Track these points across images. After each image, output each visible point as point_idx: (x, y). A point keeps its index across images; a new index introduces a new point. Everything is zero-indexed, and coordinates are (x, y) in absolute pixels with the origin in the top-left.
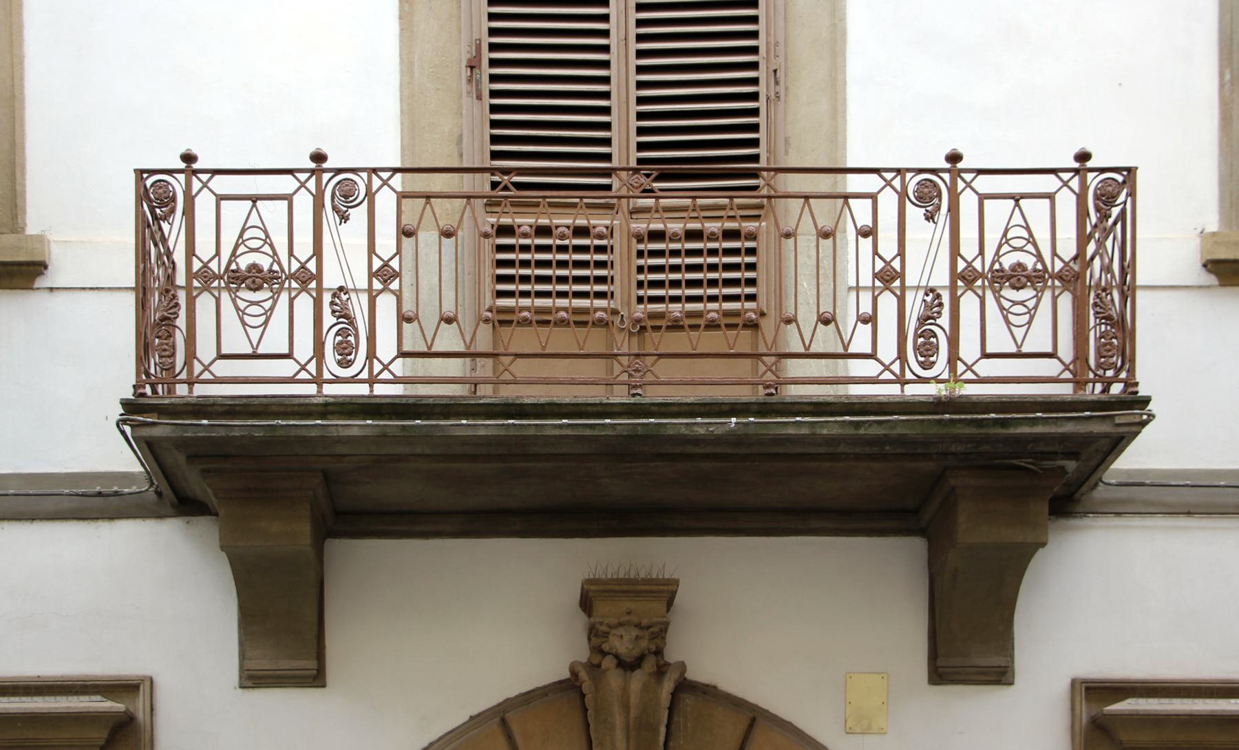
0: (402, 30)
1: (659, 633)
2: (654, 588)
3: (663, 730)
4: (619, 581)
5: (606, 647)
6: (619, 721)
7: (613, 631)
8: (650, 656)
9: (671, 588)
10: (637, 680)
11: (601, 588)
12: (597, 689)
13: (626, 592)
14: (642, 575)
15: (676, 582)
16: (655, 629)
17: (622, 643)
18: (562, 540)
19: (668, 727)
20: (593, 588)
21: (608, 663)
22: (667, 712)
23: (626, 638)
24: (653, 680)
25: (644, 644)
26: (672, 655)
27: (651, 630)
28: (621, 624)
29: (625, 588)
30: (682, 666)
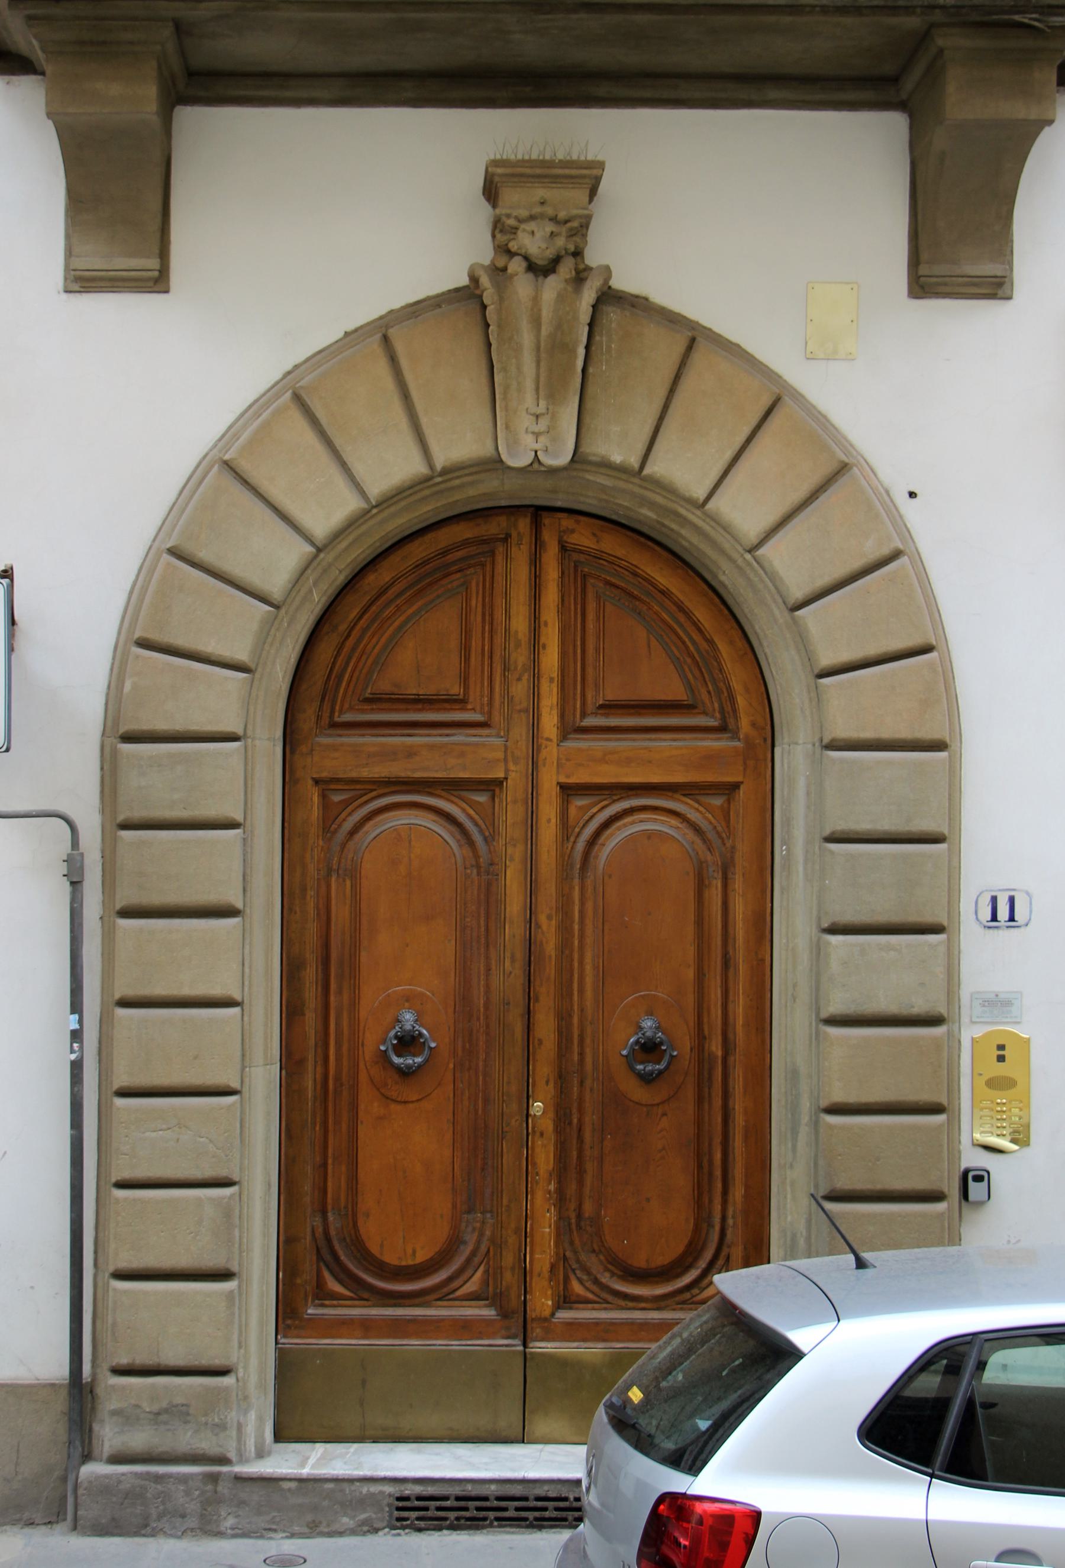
2: (574, 172)
3: (581, 351)
5: (513, 246)
6: (527, 339)
7: (523, 226)
8: (566, 259)
9: (595, 172)
10: (552, 287)
11: (509, 171)
12: (501, 299)
13: (539, 176)
15: (601, 165)
16: (575, 224)
17: (534, 242)
19: (587, 348)
20: (499, 171)
21: (516, 266)
22: (586, 329)
23: (538, 235)
24: (570, 289)
25: (561, 242)
26: (593, 257)
27: (569, 225)
28: (532, 218)
29: (538, 171)
30: (607, 271)
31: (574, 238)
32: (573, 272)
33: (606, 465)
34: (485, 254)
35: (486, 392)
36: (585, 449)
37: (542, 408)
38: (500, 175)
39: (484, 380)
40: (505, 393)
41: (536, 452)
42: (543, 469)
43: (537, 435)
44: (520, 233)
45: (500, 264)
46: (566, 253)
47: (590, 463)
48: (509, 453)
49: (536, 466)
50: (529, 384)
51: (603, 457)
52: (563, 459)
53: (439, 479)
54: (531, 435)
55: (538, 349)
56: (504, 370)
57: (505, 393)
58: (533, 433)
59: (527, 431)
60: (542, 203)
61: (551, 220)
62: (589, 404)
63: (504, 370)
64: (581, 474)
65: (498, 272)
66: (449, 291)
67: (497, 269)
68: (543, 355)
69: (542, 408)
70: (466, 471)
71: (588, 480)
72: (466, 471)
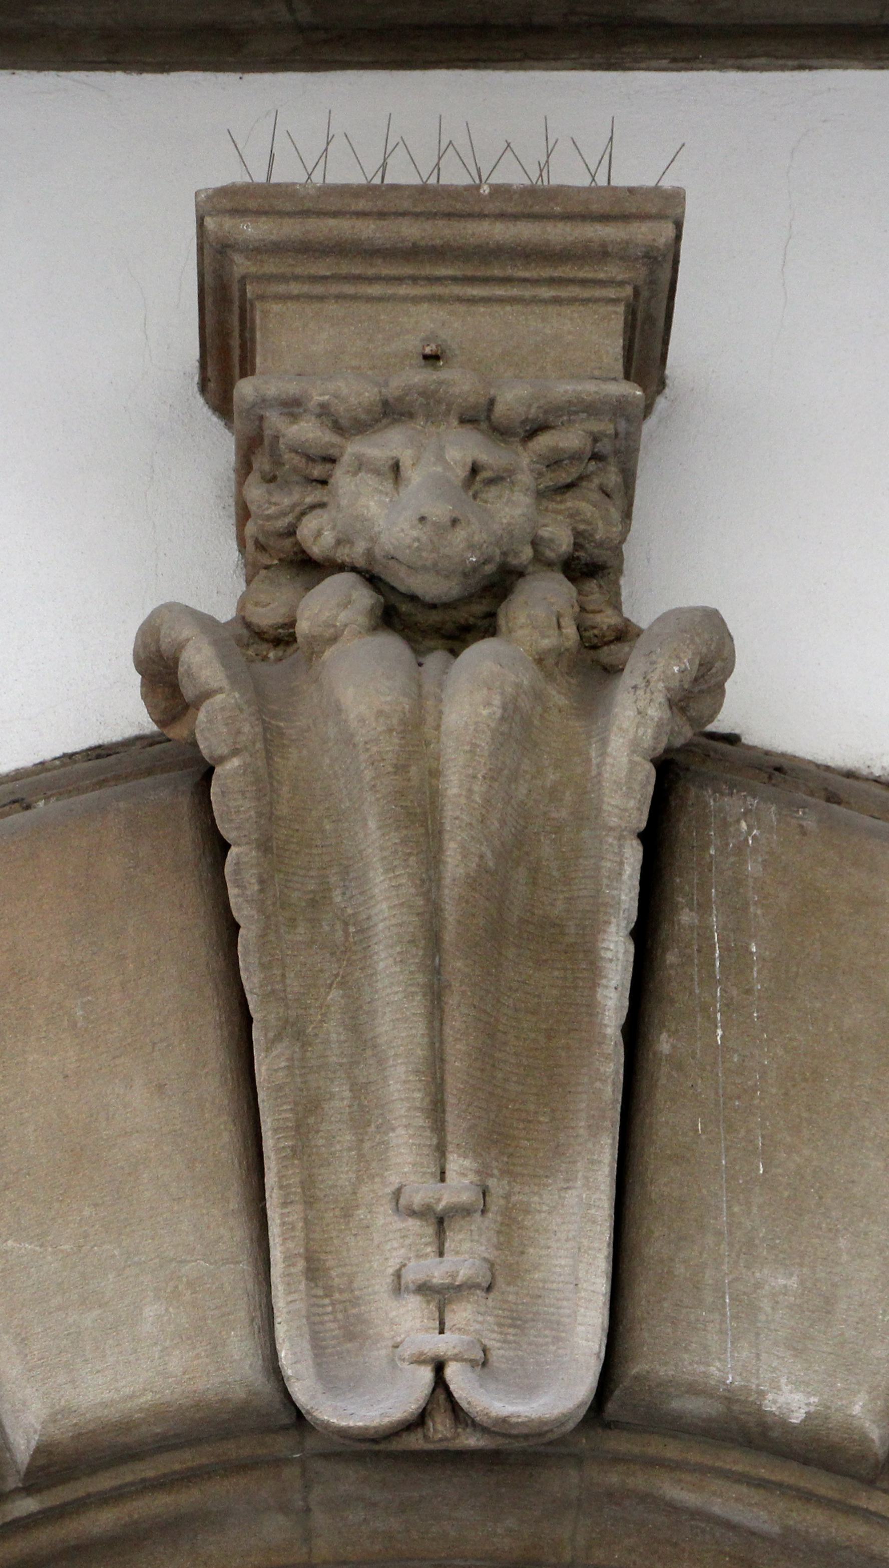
0: (538, 59)
1: (594, 463)
2: (558, 233)
3: (616, 950)
4: (378, 200)
5: (318, 535)
6: (384, 899)
7: (354, 448)
8: (546, 565)
9: (643, 233)
10: (476, 688)
11: (290, 229)
12: (272, 741)
13: (413, 253)
14: (511, 176)
15: (667, 207)
16: (569, 439)
17: (401, 505)
18: (198, 76)
19: (646, 935)
20: (250, 230)
21: (333, 605)
22: (632, 856)
23: (415, 477)
24: (557, 697)
25: (511, 509)
26: (657, 585)
27: (544, 441)
28: (392, 411)
29: (411, 231)
30: (711, 658)
31: (571, 502)
32: (570, 631)
33: (747, 1434)
34: (212, 581)
35: (222, 1138)
36: (646, 1364)
37: (460, 1181)
38: (259, 250)
39: (214, 1086)
40: (302, 1130)
41: (439, 1367)
42: (471, 1441)
43: (440, 1297)
44: (344, 481)
45: (267, 616)
46: (538, 558)
47: (678, 1428)
48: (329, 1380)
49: (441, 1427)
50: (400, 1088)
51: (730, 1398)
52: (559, 1392)
53: (28, 1505)
54: (414, 1302)
55: (433, 940)
56: (295, 1031)
57: (302, 1130)
58: (424, 1289)
59: (398, 1288)
60: (432, 359)
61: (468, 420)
62: (661, 1181)
63: (295, 1031)
64: (639, 1481)
65: (268, 642)
66: (69, 757)
67: (259, 635)
68: (456, 965)
69: (460, 1181)
70: (147, 1470)
71: (673, 1508)
72: (147, 1470)
